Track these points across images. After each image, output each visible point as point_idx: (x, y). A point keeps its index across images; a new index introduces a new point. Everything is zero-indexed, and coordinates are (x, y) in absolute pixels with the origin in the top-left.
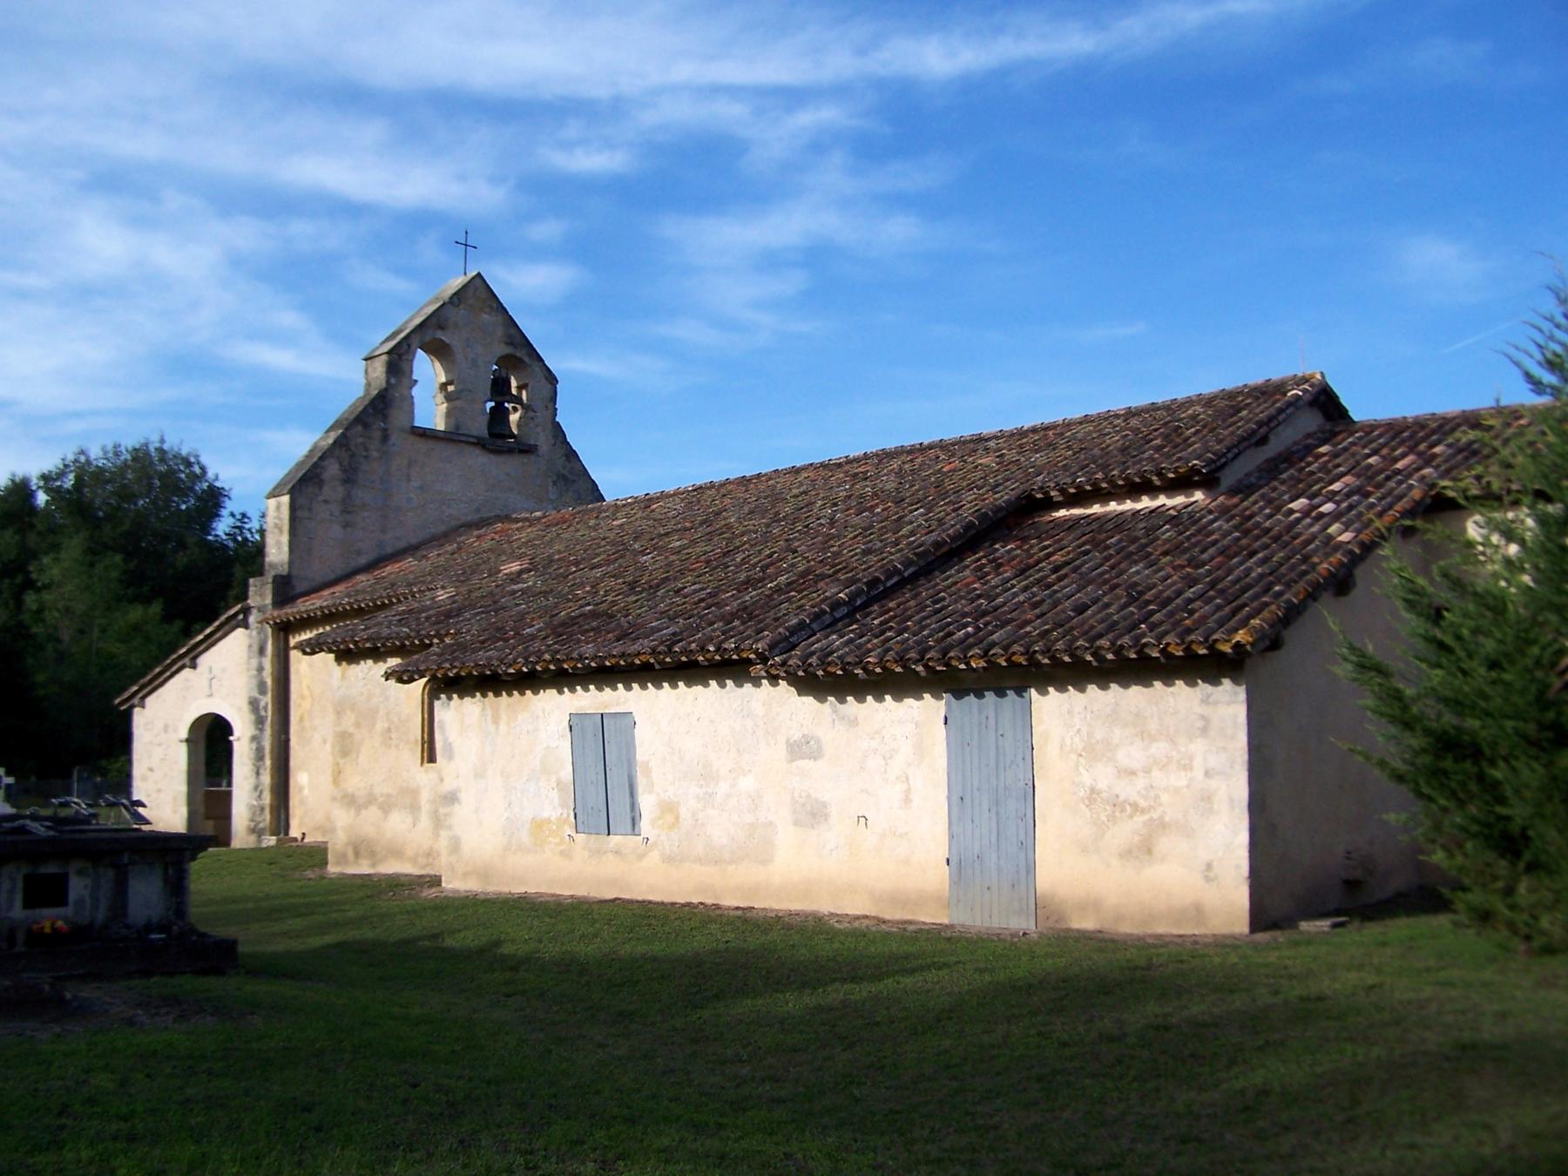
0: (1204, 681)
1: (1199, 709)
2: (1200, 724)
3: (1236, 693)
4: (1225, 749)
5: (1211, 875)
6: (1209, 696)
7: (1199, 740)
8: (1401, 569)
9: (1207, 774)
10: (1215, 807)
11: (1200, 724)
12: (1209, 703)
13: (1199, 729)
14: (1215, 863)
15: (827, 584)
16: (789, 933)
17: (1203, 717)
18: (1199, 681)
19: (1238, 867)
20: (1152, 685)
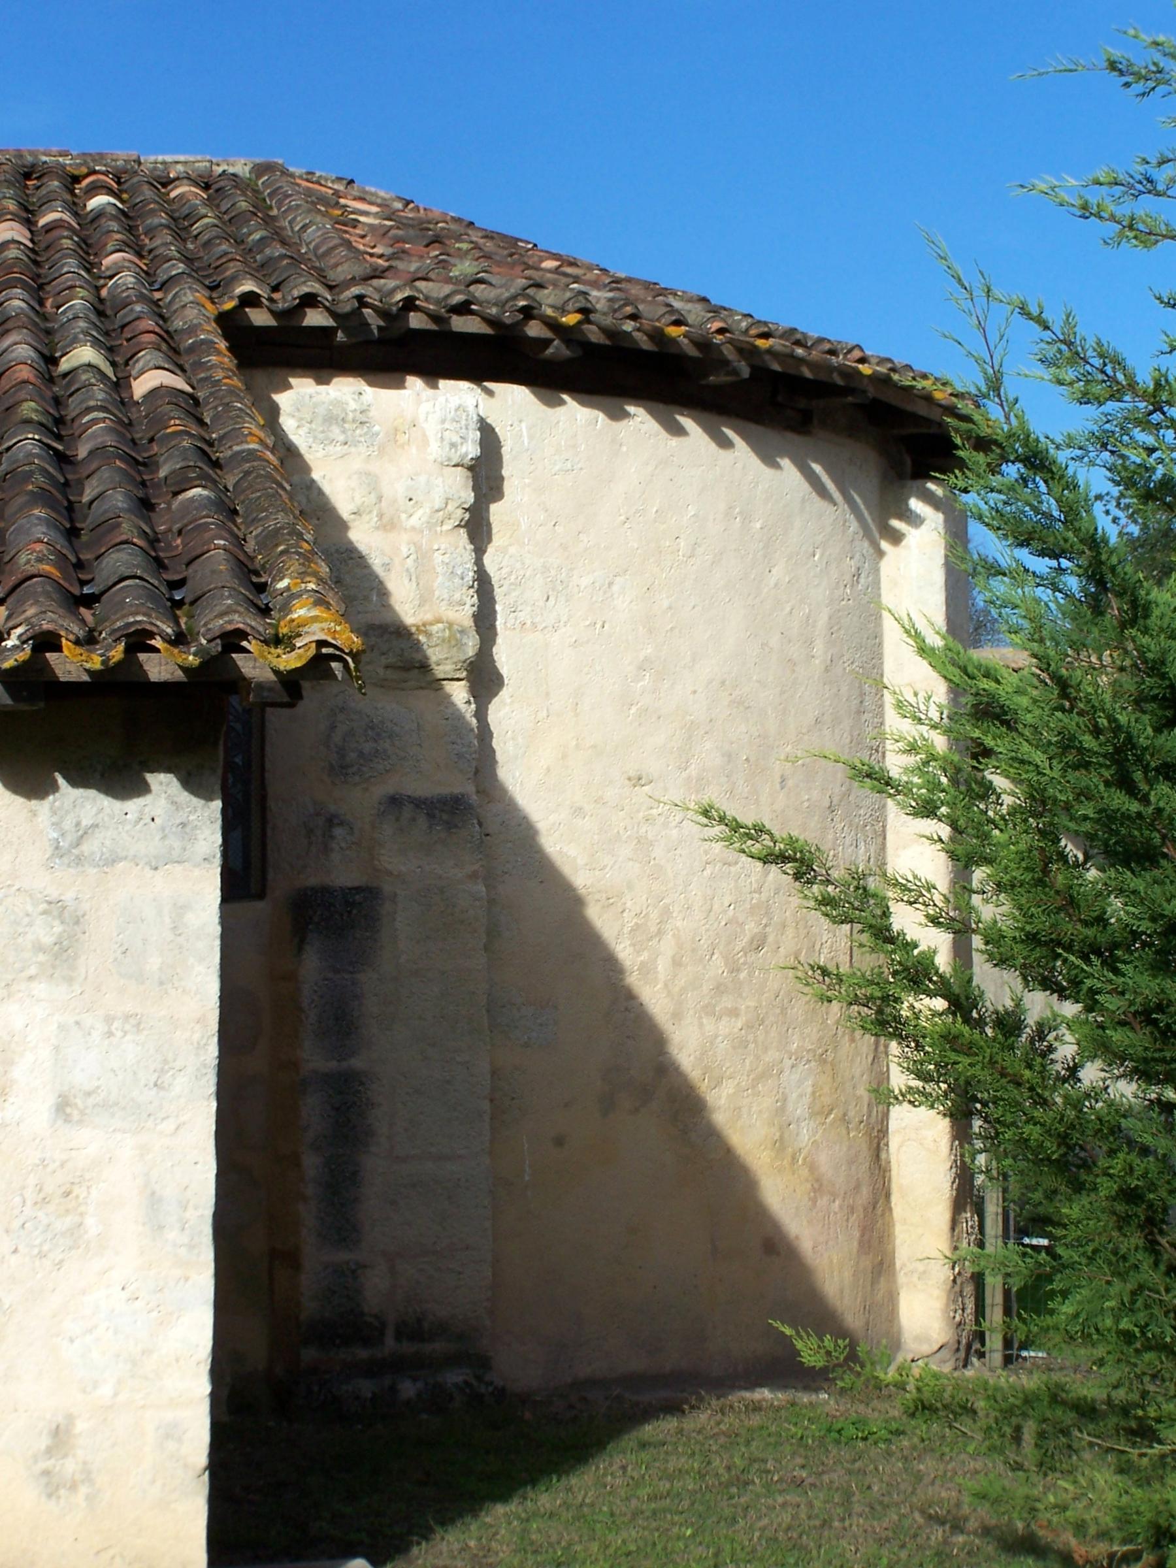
0: (75, 782)
1: (45, 883)
2: (46, 932)
3: (34, 814)
4: (136, 1022)
5: (70, 1467)
6: (84, 834)
7: (40, 989)
8: (731, 316)
9: (63, 1107)
10: (92, 1224)
11: (46, 932)
12: (79, 860)
13: (39, 948)
14: (80, 1426)
15: (129, 519)
16: (563, 1544)
17: (56, 908)
18: (61, 781)
19: (171, 1433)
20: (143, 789)
